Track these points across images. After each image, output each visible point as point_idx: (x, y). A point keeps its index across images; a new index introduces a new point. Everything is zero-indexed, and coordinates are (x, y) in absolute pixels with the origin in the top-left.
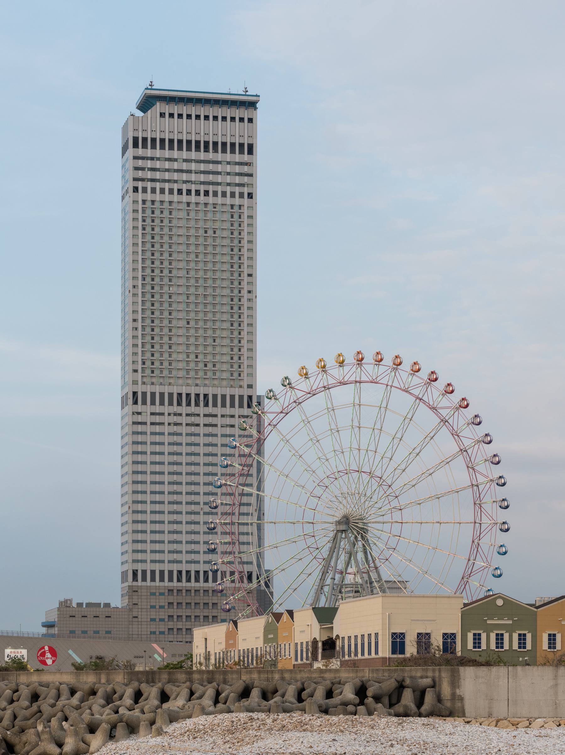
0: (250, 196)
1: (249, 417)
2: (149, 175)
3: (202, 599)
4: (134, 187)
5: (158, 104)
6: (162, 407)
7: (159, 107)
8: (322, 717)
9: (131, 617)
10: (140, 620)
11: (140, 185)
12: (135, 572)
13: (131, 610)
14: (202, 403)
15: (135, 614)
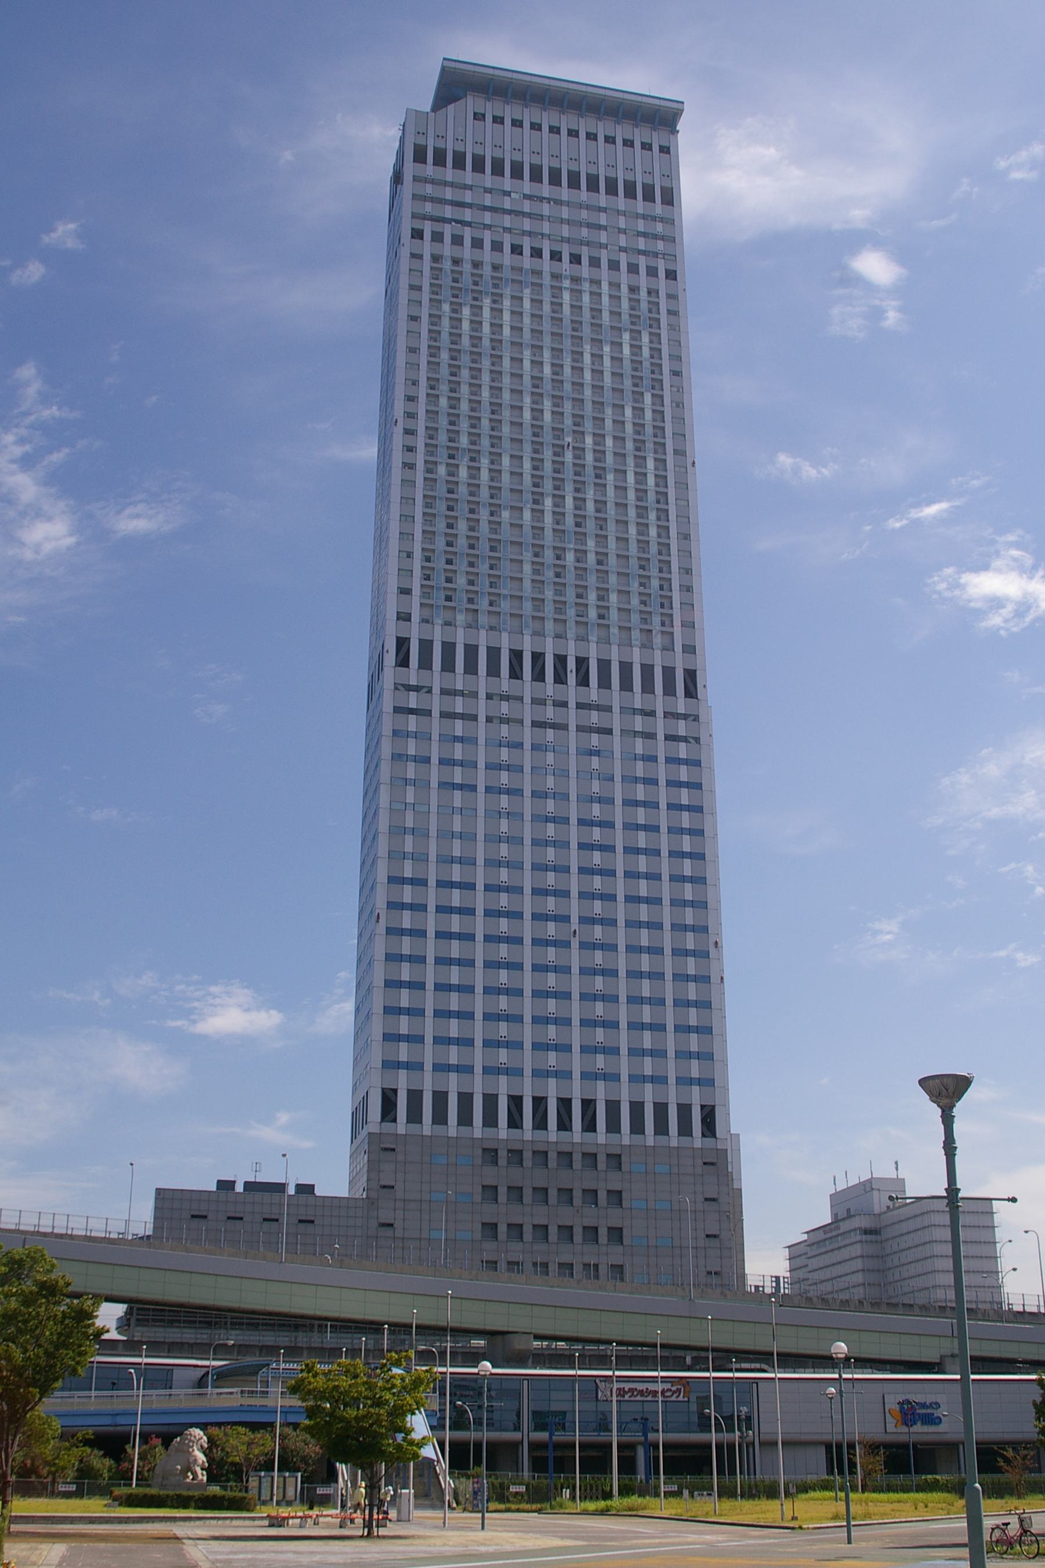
0: (671, 275)
1: (425, 690)
2: (448, 212)
3: (579, 1179)
4: (413, 229)
5: (470, 99)
6: (425, 673)
7: (472, 103)
8: (37, 1549)
9: (374, 1224)
10: (399, 1233)
11: (428, 227)
12: (391, 1094)
13: (371, 1202)
14: (572, 678)
15: (386, 1216)
